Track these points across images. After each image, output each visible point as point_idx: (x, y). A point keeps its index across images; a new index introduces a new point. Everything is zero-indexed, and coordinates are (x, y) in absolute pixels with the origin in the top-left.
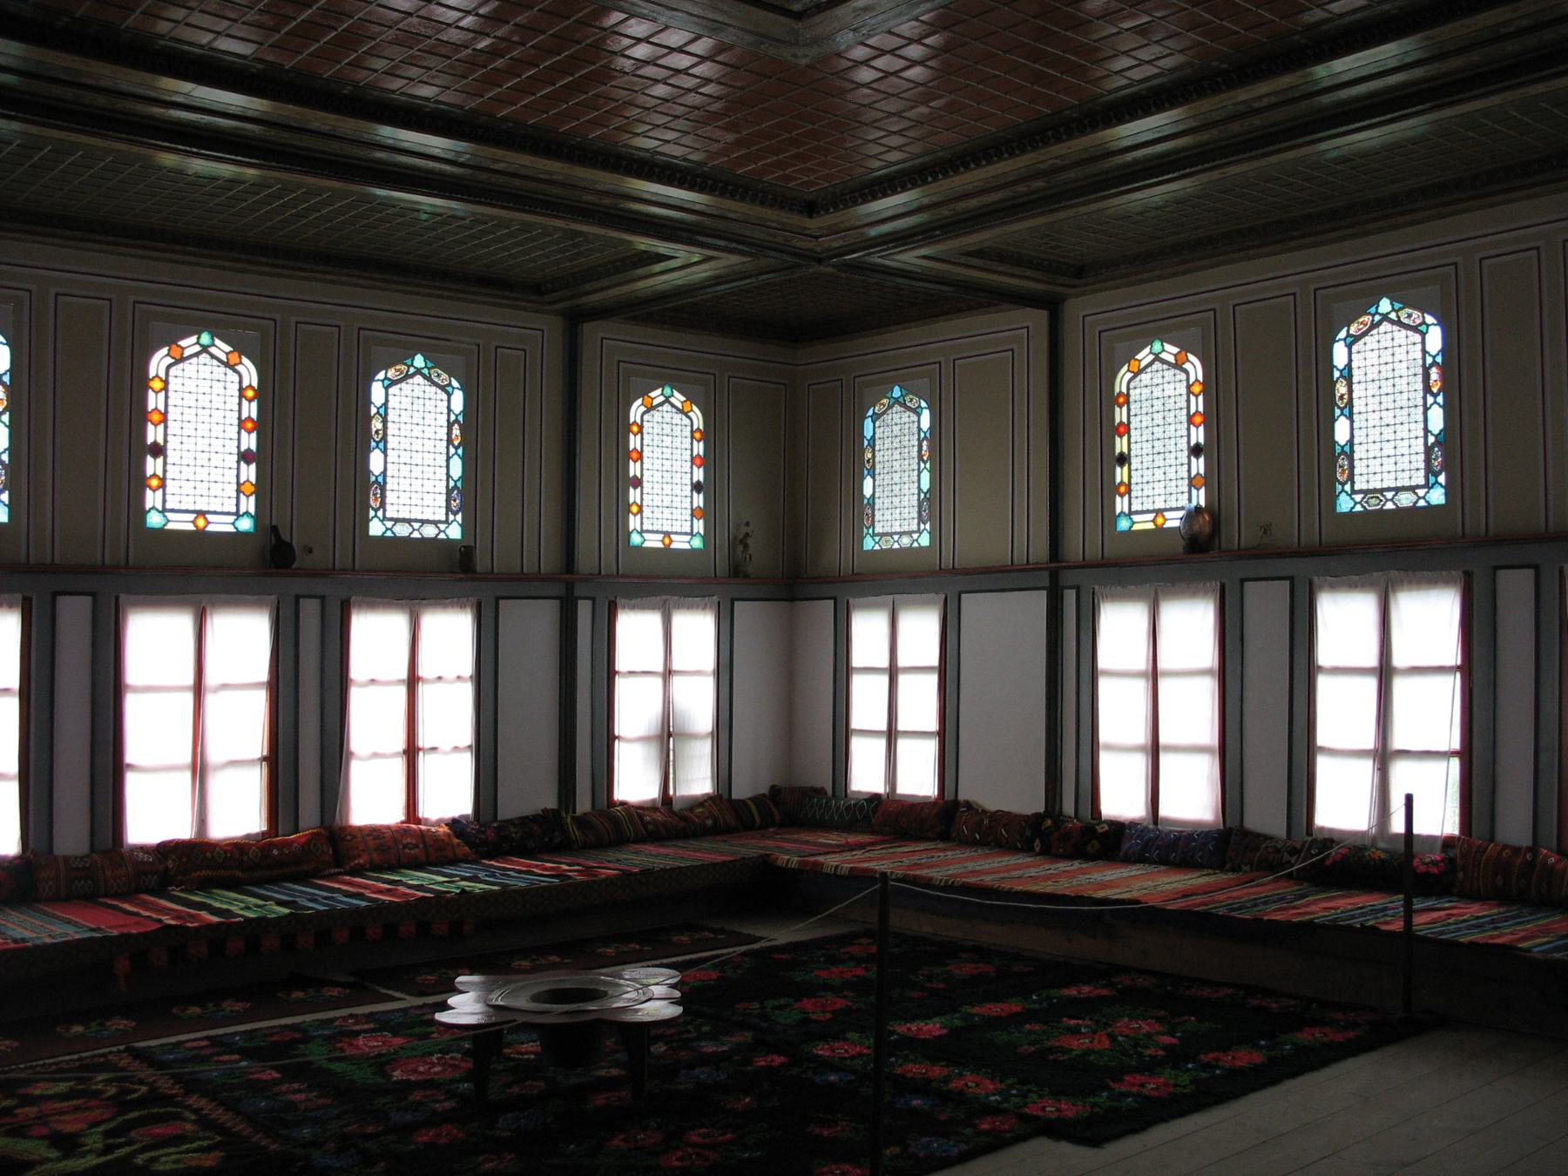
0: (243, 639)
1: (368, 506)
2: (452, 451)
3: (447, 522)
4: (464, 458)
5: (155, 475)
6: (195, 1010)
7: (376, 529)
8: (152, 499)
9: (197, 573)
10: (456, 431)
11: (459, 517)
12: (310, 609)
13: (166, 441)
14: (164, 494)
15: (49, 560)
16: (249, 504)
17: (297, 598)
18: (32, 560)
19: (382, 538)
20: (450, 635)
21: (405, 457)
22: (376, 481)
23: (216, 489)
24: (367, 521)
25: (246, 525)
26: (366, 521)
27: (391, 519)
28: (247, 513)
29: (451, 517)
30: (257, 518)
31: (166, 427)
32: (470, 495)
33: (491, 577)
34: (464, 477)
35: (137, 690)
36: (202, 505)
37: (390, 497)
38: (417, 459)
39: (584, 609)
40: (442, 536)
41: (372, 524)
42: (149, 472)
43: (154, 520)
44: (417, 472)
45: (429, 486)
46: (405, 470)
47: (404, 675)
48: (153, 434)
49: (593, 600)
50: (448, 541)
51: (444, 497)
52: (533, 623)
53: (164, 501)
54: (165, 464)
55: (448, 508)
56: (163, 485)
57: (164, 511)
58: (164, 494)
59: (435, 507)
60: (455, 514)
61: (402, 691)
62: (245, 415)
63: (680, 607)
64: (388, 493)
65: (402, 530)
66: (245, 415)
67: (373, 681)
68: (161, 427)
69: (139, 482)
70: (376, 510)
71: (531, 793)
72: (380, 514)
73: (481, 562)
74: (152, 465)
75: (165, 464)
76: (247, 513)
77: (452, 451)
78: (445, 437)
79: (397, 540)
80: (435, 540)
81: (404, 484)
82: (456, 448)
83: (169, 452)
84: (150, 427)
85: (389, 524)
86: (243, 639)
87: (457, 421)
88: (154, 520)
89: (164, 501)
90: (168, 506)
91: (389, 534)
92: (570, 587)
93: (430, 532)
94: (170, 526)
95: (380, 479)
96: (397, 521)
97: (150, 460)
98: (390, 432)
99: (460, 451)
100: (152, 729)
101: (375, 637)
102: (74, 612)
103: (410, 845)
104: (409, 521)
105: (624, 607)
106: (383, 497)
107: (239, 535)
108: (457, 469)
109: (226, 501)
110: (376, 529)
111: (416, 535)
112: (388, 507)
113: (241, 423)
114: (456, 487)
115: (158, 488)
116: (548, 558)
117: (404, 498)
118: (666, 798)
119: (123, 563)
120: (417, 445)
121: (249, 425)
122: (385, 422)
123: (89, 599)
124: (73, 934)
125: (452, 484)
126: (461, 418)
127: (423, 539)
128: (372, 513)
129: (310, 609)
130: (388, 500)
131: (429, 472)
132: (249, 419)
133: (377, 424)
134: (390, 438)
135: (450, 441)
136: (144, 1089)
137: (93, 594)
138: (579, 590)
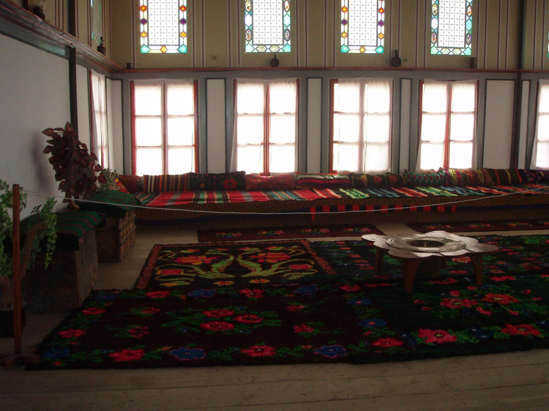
0: (379, 95)
1: (431, 42)
2: (467, 18)
3: (465, 48)
4: (473, 21)
5: (344, 32)
6: (351, 230)
7: (434, 51)
8: (343, 41)
9: (361, 70)
10: (469, 10)
11: (470, 46)
12: (406, 84)
13: (348, 19)
14: (348, 39)
15: (305, 66)
16: (382, 42)
17: (401, 79)
18: (231, 66)
19: (252, 53)
20: (465, 95)
21: (447, 21)
22: (434, 32)
23: (457, 39)
24: (430, 48)
25: (380, 50)
26: (244, 46)
27: (441, 47)
28: (381, 46)
29: (467, 46)
30: (385, 48)
31: (348, 13)
32: (476, 36)
33: (483, 71)
34: (472, 29)
35: (258, 115)
36: (363, 43)
37: (440, 38)
38: (452, 22)
39: (526, 85)
40: (462, 54)
41: (247, 47)
42: (142, 30)
43: (144, 50)
44: (452, 27)
45: (457, 33)
46: (447, 27)
47: (262, 111)
48: (344, 16)
49: (530, 81)
50: (465, 56)
51: (464, 38)
52: (501, 91)
53: (348, 42)
54: (348, 28)
55: (465, 42)
56: (347, 35)
57: (148, 45)
58: (348, 39)
59: (460, 42)
60: (469, 44)
61: (261, 119)
62: (379, 7)
63: (515, 83)
64: (439, 37)
65: (445, 52)
66: (379, 7)
67: (246, 114)
68: (146, 12)
69: (138, 34)
70: (249, 41)
71: (499, 161)
72: (436, 45)
73: (480, 65)
74: (343, 28)
75: (348, 28)
76: (381, 46)
77: (467, 18)
78: (464, 13)
79: (443, 56)
80: (459, 56)
81: (446, 33)
82: (469, 17)
83: (149, 22)
84: (342, 13)
85: (255, 47)
86: (379, 95)
87: (469, 5)
88: (144, 50)
89: (348, 42)
90: (349, 44)
91: (439, 53)
92: (519, 76)
93: (457, 52)
94: (151, 52)
95: (436, 31)
96: (443, 48)
97: (342, 26)
98: (440, 11)
99: (471, 18)
100: (344, 128)
101: (433, 95)
102: (314, 85)
103: (443, 178)
104: (448, 48)
105: (544, 84)
106: (437, 38)
107: (377, 54)
108: (469, 26)
109: (153, 40)
110: (434, 51)
111: (451, 53)
112: (439, 42)
113: (378, 10)
114: (469, 33)
115: (346, 37)
116: (510, 63)
117: (170, 36)
118: (266, 171)
119: (333, 66)
120: (452, 16)
121: (381, 11)
122: (438, 7)
123: (320, 80)
124: (293, 198)
125: (467, 32)
126: (471, 4)
127: (454, 56)
128: (432, 45)
129: (406, 84)
130: (439, 40)
131: (457, 27)
132: (183, 6)
133: (434, 8)
134: (440, 14)
135: (466, 14)
136: (304, 252)
137: (322, 78)
138: (523, 76)
